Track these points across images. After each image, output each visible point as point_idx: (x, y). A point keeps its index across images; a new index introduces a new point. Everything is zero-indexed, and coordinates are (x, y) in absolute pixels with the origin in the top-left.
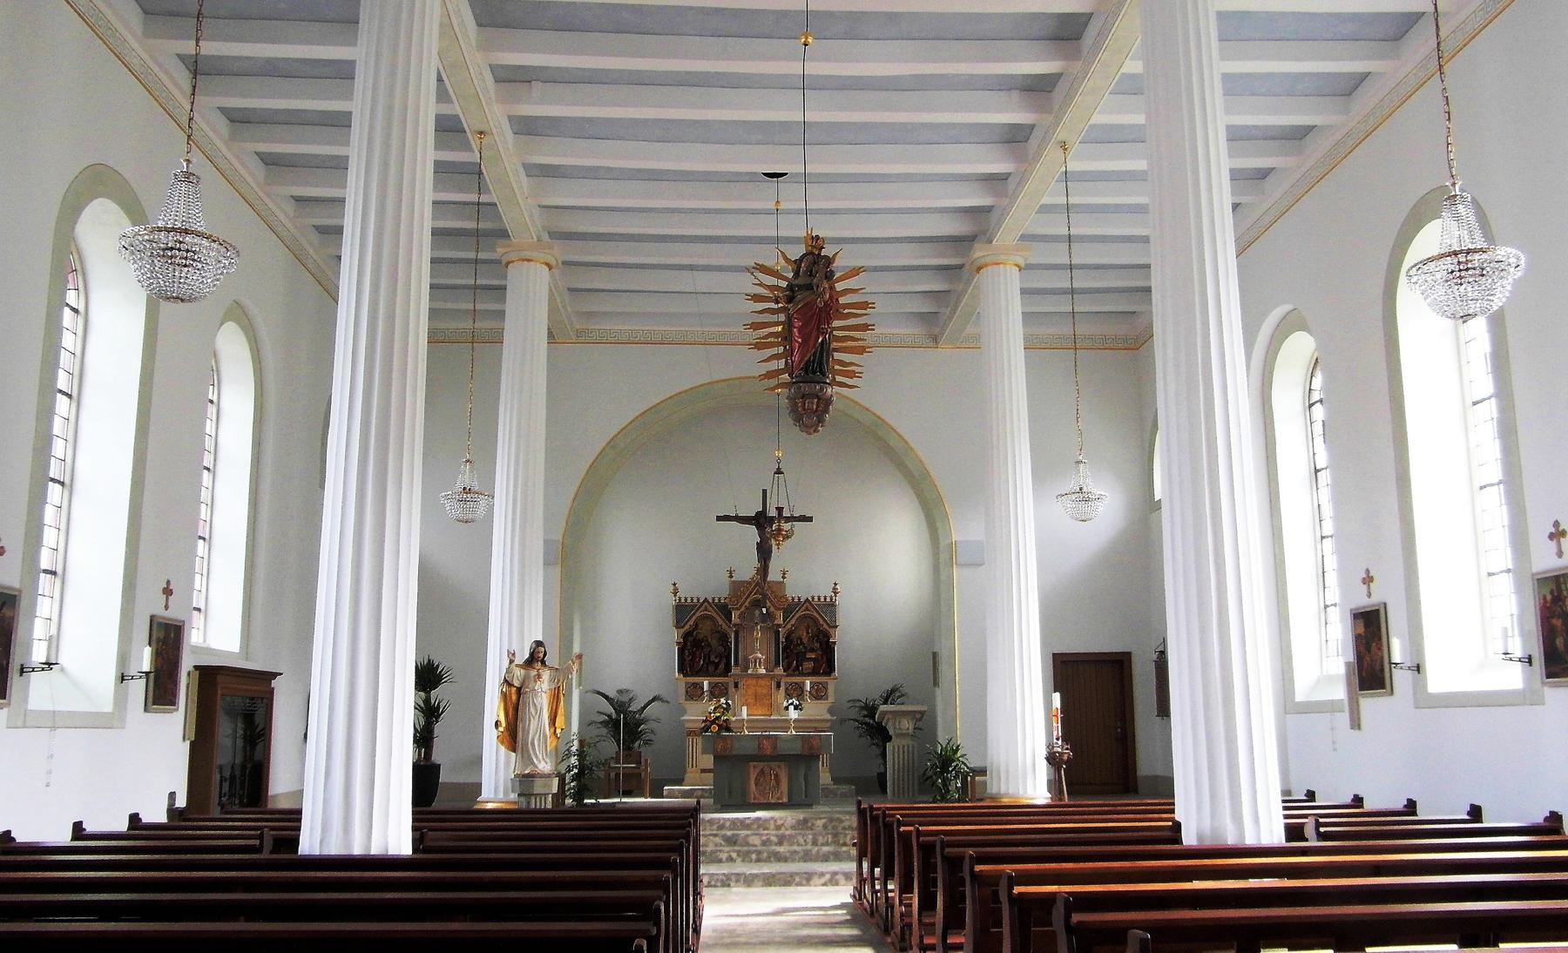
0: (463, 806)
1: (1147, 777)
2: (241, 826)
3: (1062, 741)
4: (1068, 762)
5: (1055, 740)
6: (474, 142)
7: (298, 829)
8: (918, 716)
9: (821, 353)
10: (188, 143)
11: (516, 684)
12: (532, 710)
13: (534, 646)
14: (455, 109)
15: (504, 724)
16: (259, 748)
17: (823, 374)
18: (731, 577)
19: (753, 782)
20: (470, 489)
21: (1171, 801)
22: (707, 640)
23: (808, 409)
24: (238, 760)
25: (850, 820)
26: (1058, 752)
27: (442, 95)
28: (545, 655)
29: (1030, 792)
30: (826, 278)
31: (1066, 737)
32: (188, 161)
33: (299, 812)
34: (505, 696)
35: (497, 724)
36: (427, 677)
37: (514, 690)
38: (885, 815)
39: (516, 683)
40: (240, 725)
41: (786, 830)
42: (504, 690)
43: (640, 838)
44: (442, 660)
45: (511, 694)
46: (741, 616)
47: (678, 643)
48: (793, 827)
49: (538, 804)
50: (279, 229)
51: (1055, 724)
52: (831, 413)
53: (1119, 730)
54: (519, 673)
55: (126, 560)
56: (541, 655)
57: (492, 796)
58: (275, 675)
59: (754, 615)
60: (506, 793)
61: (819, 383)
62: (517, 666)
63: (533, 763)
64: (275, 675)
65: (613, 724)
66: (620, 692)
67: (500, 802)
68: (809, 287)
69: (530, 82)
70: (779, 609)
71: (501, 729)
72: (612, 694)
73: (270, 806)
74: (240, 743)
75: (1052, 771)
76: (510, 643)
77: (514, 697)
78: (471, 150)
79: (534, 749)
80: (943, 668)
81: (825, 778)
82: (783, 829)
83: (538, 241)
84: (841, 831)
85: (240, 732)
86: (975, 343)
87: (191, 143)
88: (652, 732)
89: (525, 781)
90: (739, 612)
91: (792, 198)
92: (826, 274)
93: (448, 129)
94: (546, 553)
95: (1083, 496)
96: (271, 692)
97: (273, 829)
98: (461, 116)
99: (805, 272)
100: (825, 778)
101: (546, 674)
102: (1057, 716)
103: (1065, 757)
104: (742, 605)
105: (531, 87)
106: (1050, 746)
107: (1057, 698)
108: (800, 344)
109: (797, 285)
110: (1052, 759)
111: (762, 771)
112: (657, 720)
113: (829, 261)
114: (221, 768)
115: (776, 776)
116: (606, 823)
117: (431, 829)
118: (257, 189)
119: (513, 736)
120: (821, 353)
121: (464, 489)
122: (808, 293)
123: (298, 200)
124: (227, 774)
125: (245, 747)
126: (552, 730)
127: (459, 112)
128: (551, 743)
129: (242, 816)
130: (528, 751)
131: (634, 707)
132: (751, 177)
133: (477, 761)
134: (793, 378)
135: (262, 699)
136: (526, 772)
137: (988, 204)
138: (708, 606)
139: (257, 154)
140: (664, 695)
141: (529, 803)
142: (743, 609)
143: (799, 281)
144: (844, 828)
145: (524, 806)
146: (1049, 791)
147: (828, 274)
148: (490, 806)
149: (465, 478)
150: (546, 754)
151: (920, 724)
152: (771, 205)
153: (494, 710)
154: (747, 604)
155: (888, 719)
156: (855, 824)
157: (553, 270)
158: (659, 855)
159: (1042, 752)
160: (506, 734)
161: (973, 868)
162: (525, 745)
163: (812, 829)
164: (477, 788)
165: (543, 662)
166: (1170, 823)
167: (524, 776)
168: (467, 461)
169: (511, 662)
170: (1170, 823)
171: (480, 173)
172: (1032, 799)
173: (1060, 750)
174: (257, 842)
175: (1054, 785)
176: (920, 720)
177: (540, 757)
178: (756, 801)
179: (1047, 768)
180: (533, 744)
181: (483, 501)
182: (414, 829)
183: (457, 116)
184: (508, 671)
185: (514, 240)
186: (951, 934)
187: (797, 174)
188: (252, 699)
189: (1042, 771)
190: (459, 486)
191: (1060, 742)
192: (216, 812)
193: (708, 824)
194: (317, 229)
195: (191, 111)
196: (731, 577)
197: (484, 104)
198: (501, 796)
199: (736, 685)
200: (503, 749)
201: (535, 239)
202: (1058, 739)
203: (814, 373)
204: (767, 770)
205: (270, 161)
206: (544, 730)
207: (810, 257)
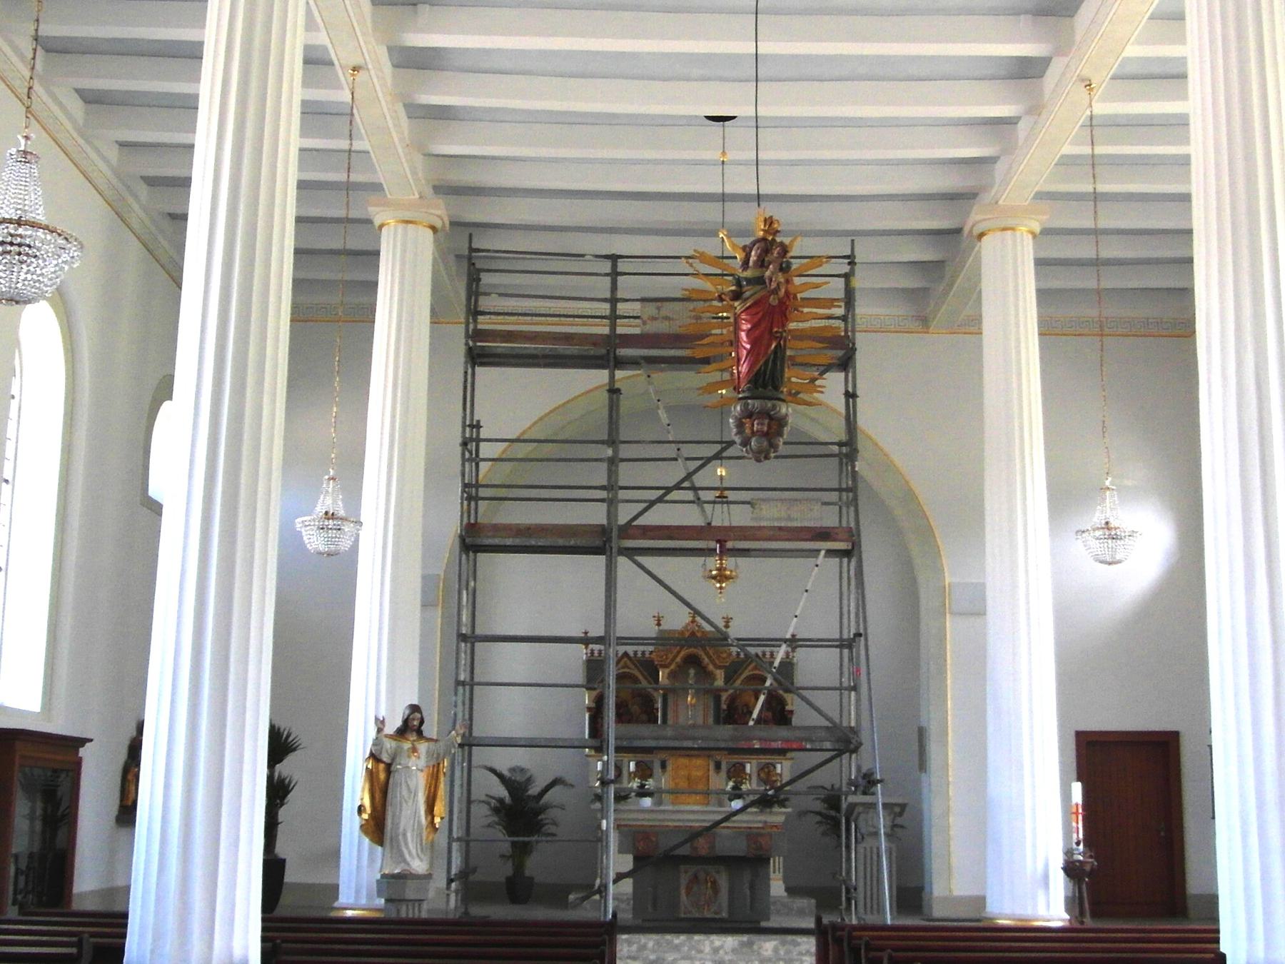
0: (322, 914)
1: (1196, 896)
2: (49, 931)
3: (1084, 846)
4: (1092, 873)
5: (1075, 846)
6: (343, 77)
7: (124, 936)
8: (897, 810)
9: (774, 362)
10: (27, 117)
11: (385, 759)
12: (405, 793)
13: (407, 712)
14: (322, 38)
15: (368, 810)
16: (62, 835)
17: (776, 388)
18: (659, 624)
19: (683, 892)
20: (333, 514)
21: (1214, 927)
22: (627, 706)
23: (757, 431)
24: (36, 847)
25: (808, 943)
26: (1079, 861)
27: (310, 25)
28: (422, 722)
29: (1042, 911)
30: (781, 269)
31: (1089, 840)
32: (27, 138)
33: (125, 916)
34: (371, 775)
35: (361, 810)
36: (280, 746)
37: (382, 766)
38: (850, 937)
39: (385, 758)
40: (39, 805)
41: (726, 953)
42: (370, 766)
43: (438, 944)
44: (296, 728)
45: (378, 772)
46: (672, 675)
47: (589, 709)
48: (734, 950)
49: (411, 911)
50: (94, 175)
51: (1074, 824)
52: (785, 437)
53: (1162, 834)
54: (389, 745)
55: (144, 709)
56: (416, 723)
57: (351, 901)
58: (82, 742)
59: (689, 674)
60: (369, 897)
61: (770, 399)
62: (386, 736)
63: (405, 861)
64: (82, 742)
65: (500, 809)
66: (513, 770)
67: (363, 910)
68: (759, 281)
69: (415, 5)
70: (720, 667)
71: (365, 816)
72: (506, 773)
73: (76, 905)
74: (38, 826)
75: (1071, 885)
76: (377, 708)
77: (382, 776)
78: (340, 87)
79: (406, 844)
80: (933, 749)
81: (777, 887)
82: (721, 952)
83: (421, 197)
84: (796, 957)
85: (39, 812)
86: (973, 325)
87: (29, 115)
88: (555, 824)
89: (393, 884)
90: (667, 671)
91: (739, 145)
92: (781, 265)
93: (315, 61)
94: (424, 592)
95: (1110, 532)
96: (79, 763)
97: (93, 935)
98: (330, 46)
99: (755, 263)
100: (777, 887)
101: (423, 747)
102: (1077, 813)
103: (1088, 868)
104: (673, 660)
105: (416, 12)
106: (1069, 853)
107: (1077, 789)
108: (749, 352)
109: (746, 279)
110: (1071, 869)
111: (696, 877)
112: (562, 807)
113: (785, 250)
114: (16, 857)
115: (714, 883)
116: (565, 950)
117: (285, 941)
118: (75, 135)
119: (377, 827)
120: (774, 362)
121: (326, 513)
122: (758, 287)
123: (123, 145)
124: (23, 866)
125: (43, 832)
126: (429, 818)
127: (327, 42)
128: (428, 837)
129: (48, 919)
130: (398, 842)
131: (534, 790)
132: (689, 121)
133: (334, 855)
134: (739, 393)
135: (68, 771)
136: (396, 871)
137: (1012, 115)
138: (628, 662)
139: (77, 90)
140: (570, 778)
141: (398, 911)
142: (673, 667)
143: (748, 274)
144: (801, 954)
145: (393, 915)
146: (1068, 910)
147: (784, 265)
148: (349, 913)
149: (326, 502)
150: (422, 849)
151: (899, 821)
152: (717, 155)
153: (356, 791)
154: (678, 659)
155: (859, 813)
156: (813, 949)
157: (439, 234)
158: (110, 940)
159: (1058, 861)
160: (372, 823)
161: (78, 952)
162: (394, 840)
163: (782, 804)
164: (334, 890)
165: (420, 733)
166: (1213, 955)
167: (394, 876)
168: (329, 479)
169: (379, 730)
170: (1213, 955)
171: (352, 114)
172: (1049, 921)
173: (1081, 858)
174: (74, 950)
175: (1074, 904)
176: (901, 814)
177: (414, 852)
178: (688, 916)
179: (1065, 879)
180: (404, 835)
181: (347, 528)
182: (264, 940)
183: (325, 48)
184: (377, 743)
185: (389, 196)
186: (460, 846)
187: (746, 118)
188: (55, 771)
189: (1059, 885)
190: (320, 509)
191: (1081, 847)
192: (12, 912)
193: (625, 945)
194: (81, 97)
195: (31, 78)
196: (659, 624)
197: (359, 34)
198: (363, 901)
199: (663, 766)
200: (366, 841)
201: (417, 196)
202: (1078, 844)
203: (765, 386)
204: (702, 876)
205: (91, 98)
206: (419, 817)
207: (762, 244)
